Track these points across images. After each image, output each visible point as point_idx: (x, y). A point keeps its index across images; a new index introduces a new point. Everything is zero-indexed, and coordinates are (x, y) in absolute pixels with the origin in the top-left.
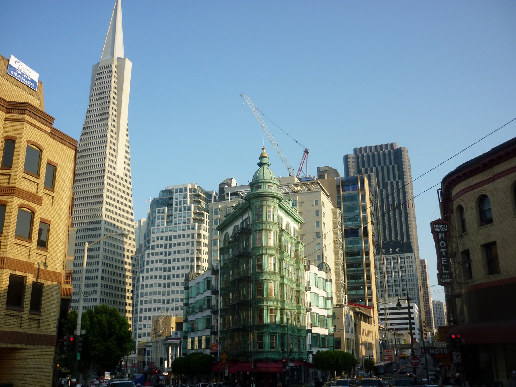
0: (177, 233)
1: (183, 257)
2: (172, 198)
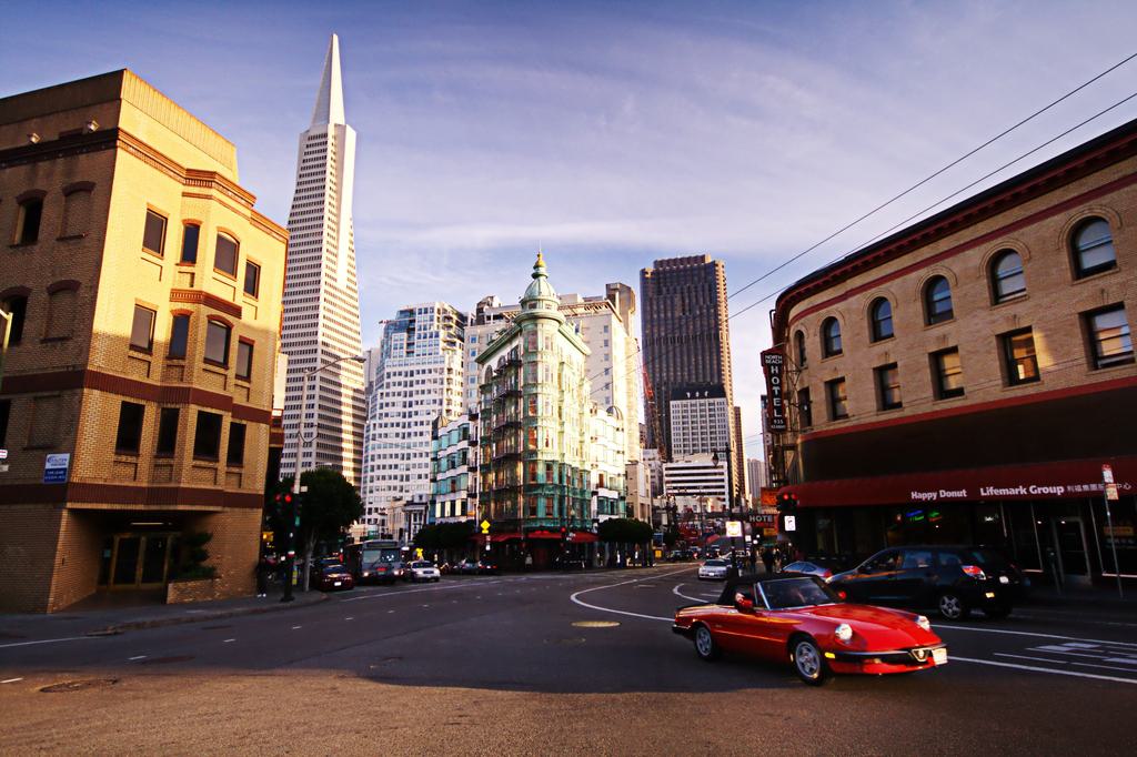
0: (421, 368)
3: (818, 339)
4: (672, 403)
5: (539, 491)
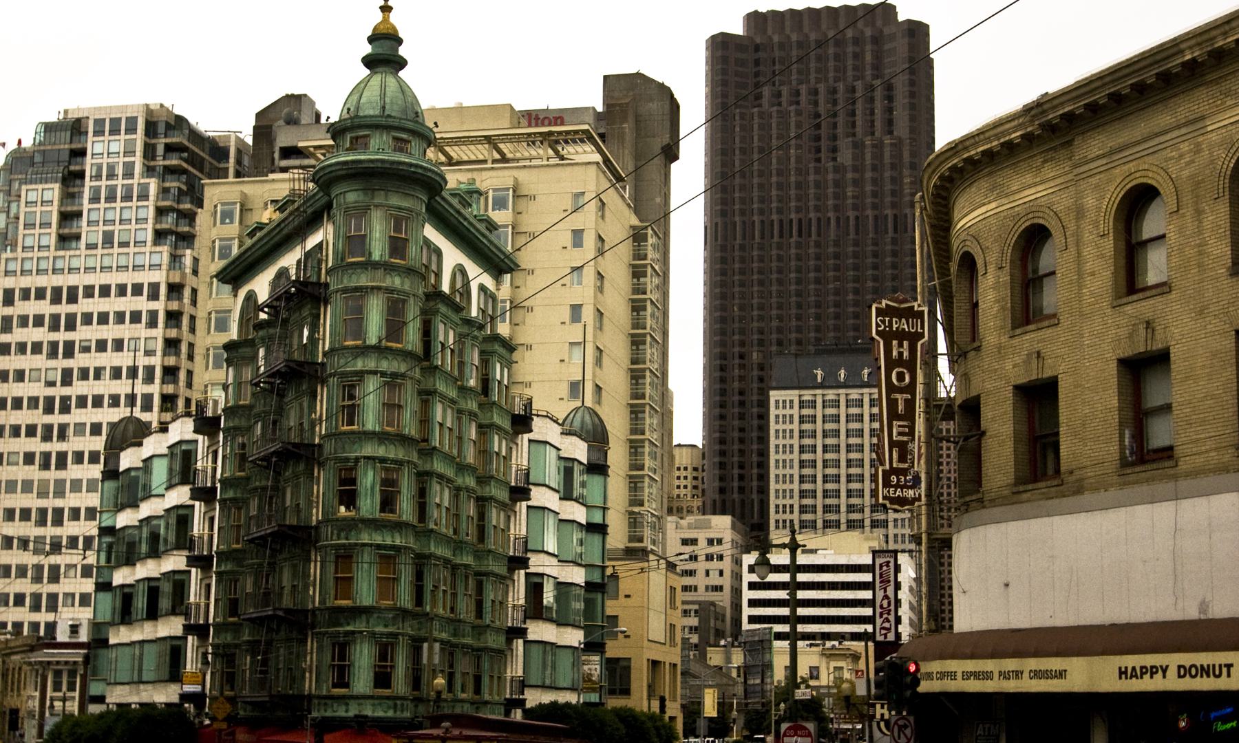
0: (97, 280)
1: (116, 363)
2: (82, 153)
3: (1109, 244)
4: (774, 395)
5: (359, 626)
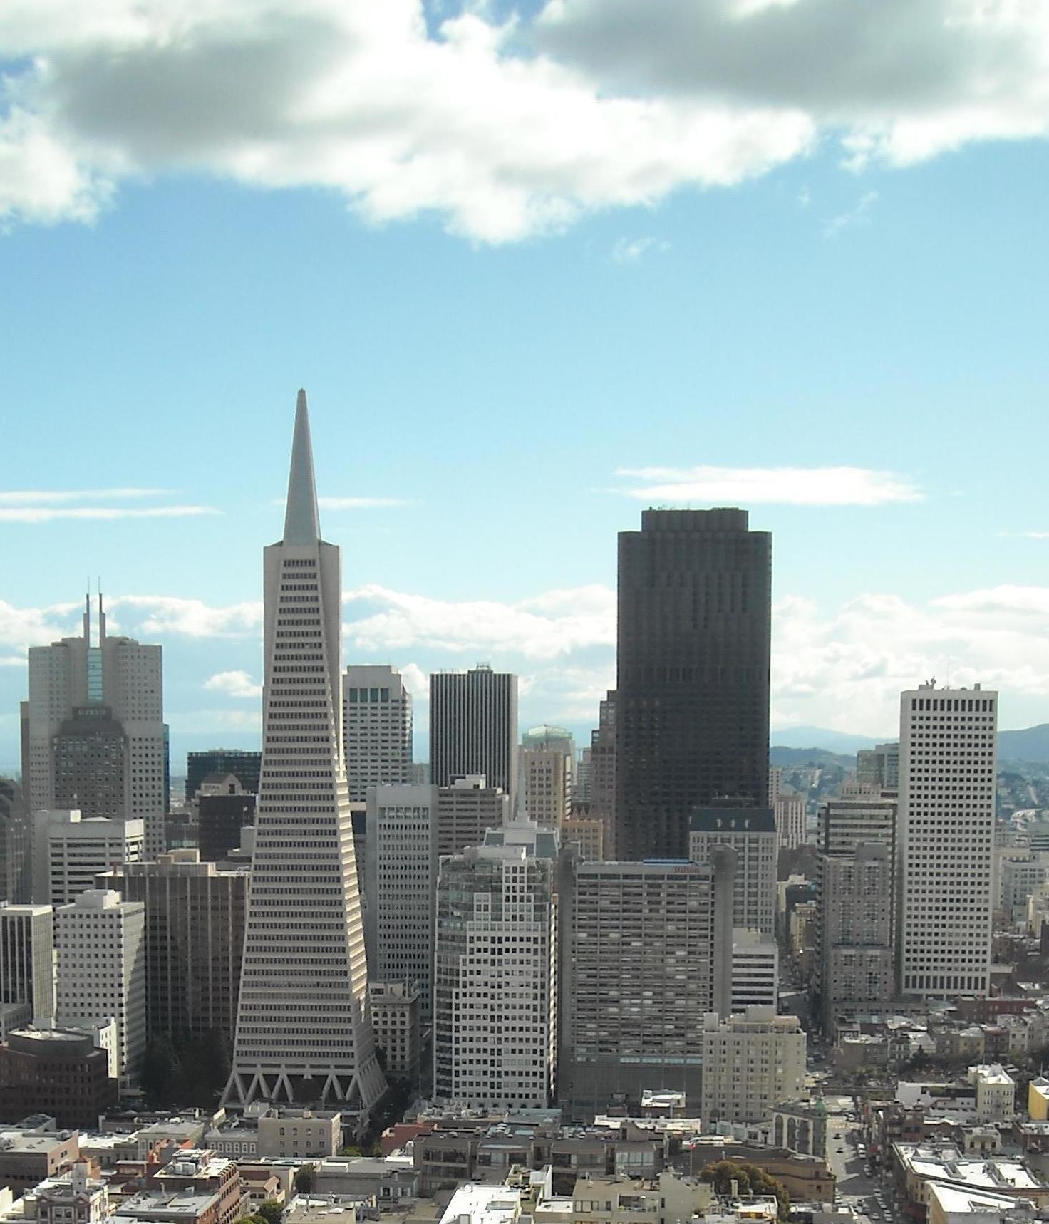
4: (692, 834)
